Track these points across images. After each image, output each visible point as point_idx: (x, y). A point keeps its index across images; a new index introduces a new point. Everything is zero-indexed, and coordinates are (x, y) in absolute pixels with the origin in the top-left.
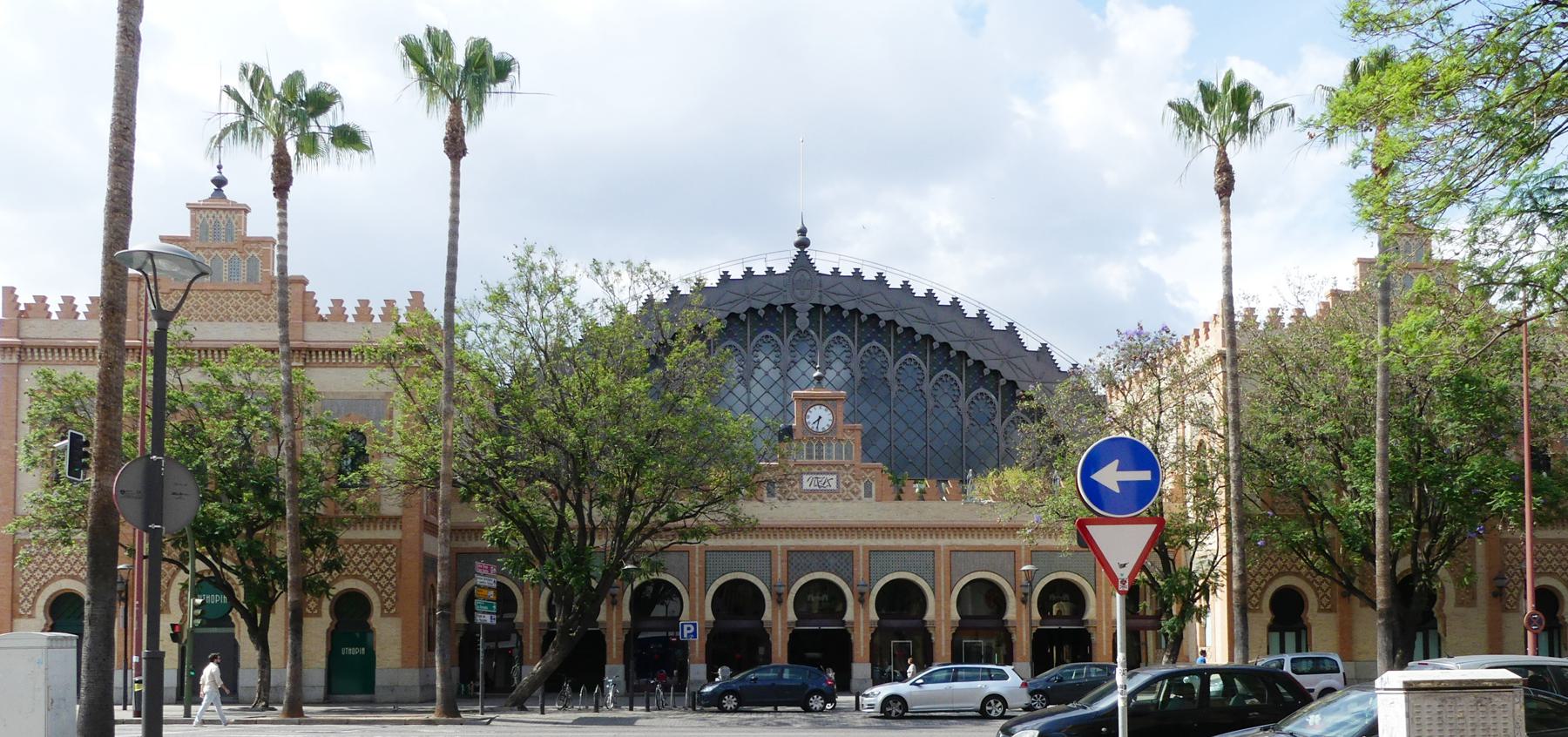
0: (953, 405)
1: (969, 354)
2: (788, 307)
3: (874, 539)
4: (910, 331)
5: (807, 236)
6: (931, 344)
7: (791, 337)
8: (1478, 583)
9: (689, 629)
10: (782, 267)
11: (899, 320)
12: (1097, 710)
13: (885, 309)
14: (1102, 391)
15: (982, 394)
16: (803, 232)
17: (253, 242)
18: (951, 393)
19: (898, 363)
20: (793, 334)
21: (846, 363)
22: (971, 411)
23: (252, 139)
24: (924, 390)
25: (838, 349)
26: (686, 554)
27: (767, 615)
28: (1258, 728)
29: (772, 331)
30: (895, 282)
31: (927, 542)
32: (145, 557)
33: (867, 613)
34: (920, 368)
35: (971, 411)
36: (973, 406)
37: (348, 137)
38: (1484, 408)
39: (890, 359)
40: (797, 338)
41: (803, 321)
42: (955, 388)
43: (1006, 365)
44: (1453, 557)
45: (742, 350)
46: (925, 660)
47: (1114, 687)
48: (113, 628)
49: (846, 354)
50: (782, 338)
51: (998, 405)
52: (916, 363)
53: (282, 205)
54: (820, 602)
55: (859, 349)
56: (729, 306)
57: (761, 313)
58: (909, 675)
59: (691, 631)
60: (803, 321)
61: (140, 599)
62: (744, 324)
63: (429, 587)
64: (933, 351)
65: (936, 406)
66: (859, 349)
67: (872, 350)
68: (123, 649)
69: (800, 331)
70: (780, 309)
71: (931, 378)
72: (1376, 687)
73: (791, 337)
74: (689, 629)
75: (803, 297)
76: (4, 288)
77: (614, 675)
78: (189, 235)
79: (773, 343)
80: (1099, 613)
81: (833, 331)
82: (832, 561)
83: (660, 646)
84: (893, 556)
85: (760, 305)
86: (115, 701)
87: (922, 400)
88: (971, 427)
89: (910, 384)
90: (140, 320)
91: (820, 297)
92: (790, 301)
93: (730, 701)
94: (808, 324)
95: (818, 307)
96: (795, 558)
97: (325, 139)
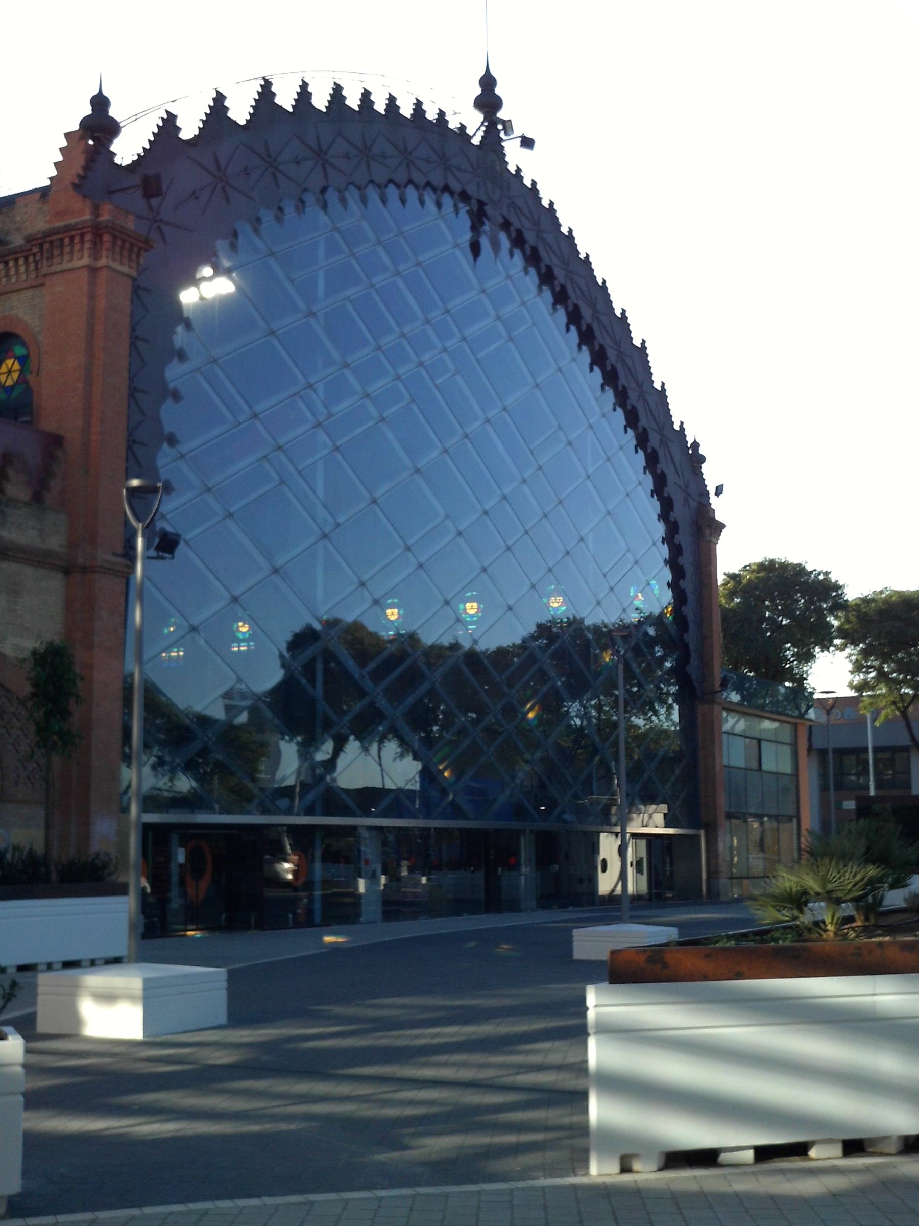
8: (14, 840)
12: (676, 829)
14: (367, 677)
16: (488, 82)
17: (205, 622)
23: (504, 1178)
28: (601, 876)
30: (59, 158)
32: (614, 774)
37: (395, 759)
38: (29, 779)
44: (85, 201)
46: (372, 703)
47: (832, 923)
48: (202, 966)
53: (641, 1172)
54: (824, 922)
58: (20, 420)
61: (417, 1037)
63: (681, 475)
68: (208, 1032)
72: (471, 134)
76: (724, 526)
77: (227, 702)
78: (600, 893)
83: (826, 642)
84: (123, 601)
86: (637, 841)
90: (140, 634)
92: (484, 198)
97: (473, 202)
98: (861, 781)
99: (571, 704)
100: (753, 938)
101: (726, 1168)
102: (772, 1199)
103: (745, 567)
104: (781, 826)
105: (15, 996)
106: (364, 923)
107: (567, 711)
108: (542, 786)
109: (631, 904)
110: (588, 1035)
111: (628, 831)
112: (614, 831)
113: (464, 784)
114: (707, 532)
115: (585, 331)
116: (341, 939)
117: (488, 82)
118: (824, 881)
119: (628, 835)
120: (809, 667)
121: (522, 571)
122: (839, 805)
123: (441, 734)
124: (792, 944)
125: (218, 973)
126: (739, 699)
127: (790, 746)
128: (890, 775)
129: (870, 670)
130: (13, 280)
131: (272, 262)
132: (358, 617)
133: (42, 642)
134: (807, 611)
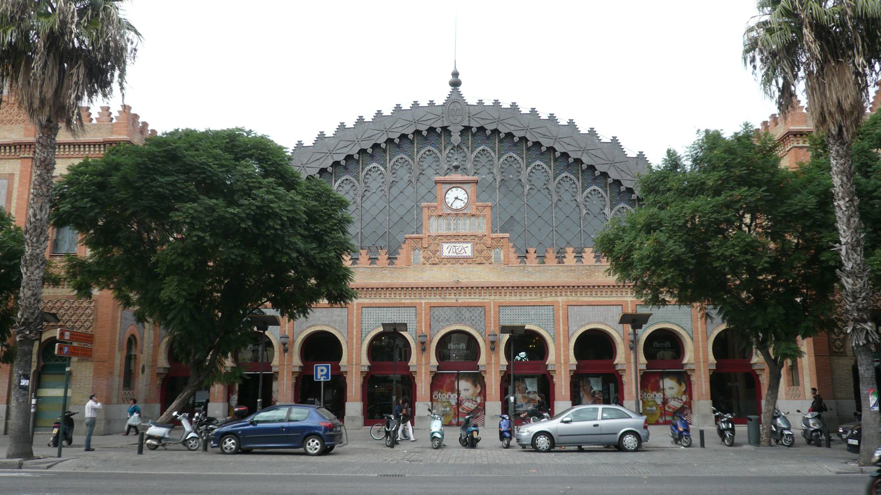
0: (573, 199)
1: (584, 161)
2: (445, 129)
3: (477, 297)
4: (537, 144)
5: (459, 77)
6: (554, 154)
7: (447, 151)
9: (322, 371)
10: (440, 101)
11: (557, 147)
13: (488, 121)
15: (594, 190)
16: (455, 74)
18: (571, 190)
19: (529, 169)
20: (450, 147)
21: (489, 169)
22: (587, 204)
24: (550, 188)
25: (483, 159)
26: (413, 310)
27: (413, 361)
29: (434, 147)
31: (475, 299)
33: (428, 358)
34: (546, 172)
35: (587, 204)
36: (587, 199)
39: (523, 166)
40: (452, 151)
41: (456, 138)
42: (574, 186)
43: (418, 125)
45: (410, 160)
49: (489, 163)
50: (441, 151)
51: (607, 199)
52: (543, 168)
55: (499, 158)
56: (402, 128)
57: (425, 133)
59: (324, 373)
60: (456, 138)
62: (412, 142)
64: (556, 160)
65: (560, 200)
66: (499, 158)
67: (509, 159)
69: (454, 146)
70: (439, 130)
71: (555, 178)
73: (447, 151)
74: (322, 371)
75: (456, 122)
79: (434, 155)
80: (697, 358)
81: (507, 151)
82: (467, 314)
85: (423, 128)
87: (549, 197)
88: (587, 215)
89: (539, 184)
91: (469, 121)
92: (445, 125)
93: (230, 443)
94: (460, 140)
95: (467, 129)
96: (437, 313)
98: (727, 269)
99: (187, 278)
100: (760, 245)
101: (629, 453)
102: (652, 414)
103: (694, 142)
104: (459, 222)
105: (236, 128)
106: (691, 397)
107: (757, 218)
108: (318, 239)
109: (185, 134)
110: (819, 412)
111: (316, 399)
112: (859, 358)
113: (529, 153)
114: (50, 95)
115: (796, 335)
116: (244, 408)
117: (455, 74)
118: (745, 241)
119: (313, 399)
120: (859, 253)
121: (389, 473)
122: (457, 214)
123: (535, 343)
124: (8, 460)
125: (267, 333)
126: (331, 398)
127: (459, 382)
128: (692, 264)
129: (871, 339)
130: (8, 154)
131: (834, 149)
132: (457, 447)
133: (859, 146)
134: (743, 207)
